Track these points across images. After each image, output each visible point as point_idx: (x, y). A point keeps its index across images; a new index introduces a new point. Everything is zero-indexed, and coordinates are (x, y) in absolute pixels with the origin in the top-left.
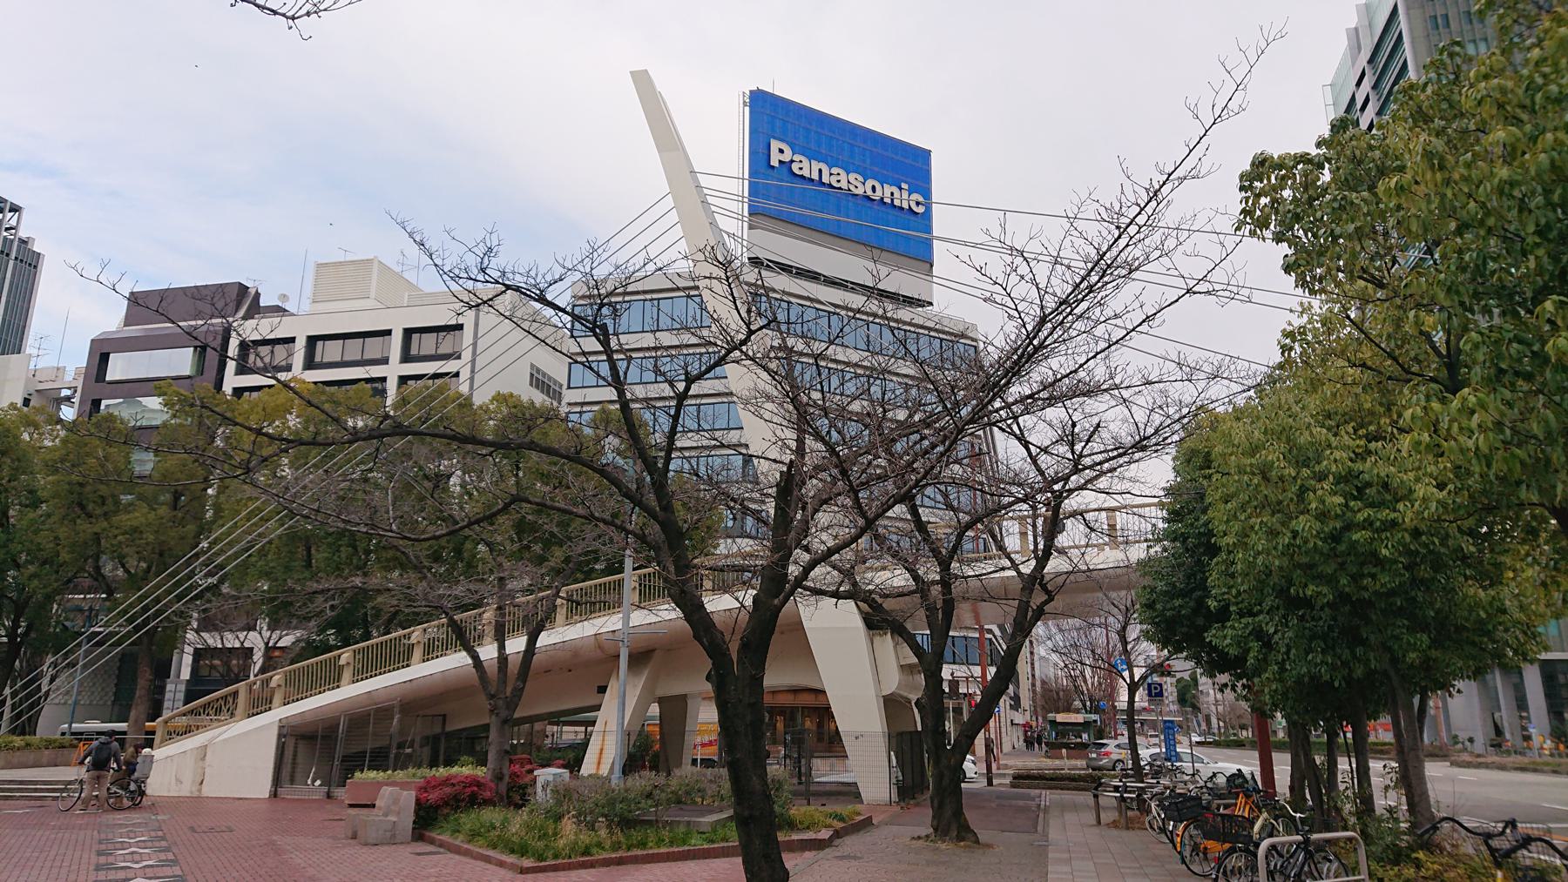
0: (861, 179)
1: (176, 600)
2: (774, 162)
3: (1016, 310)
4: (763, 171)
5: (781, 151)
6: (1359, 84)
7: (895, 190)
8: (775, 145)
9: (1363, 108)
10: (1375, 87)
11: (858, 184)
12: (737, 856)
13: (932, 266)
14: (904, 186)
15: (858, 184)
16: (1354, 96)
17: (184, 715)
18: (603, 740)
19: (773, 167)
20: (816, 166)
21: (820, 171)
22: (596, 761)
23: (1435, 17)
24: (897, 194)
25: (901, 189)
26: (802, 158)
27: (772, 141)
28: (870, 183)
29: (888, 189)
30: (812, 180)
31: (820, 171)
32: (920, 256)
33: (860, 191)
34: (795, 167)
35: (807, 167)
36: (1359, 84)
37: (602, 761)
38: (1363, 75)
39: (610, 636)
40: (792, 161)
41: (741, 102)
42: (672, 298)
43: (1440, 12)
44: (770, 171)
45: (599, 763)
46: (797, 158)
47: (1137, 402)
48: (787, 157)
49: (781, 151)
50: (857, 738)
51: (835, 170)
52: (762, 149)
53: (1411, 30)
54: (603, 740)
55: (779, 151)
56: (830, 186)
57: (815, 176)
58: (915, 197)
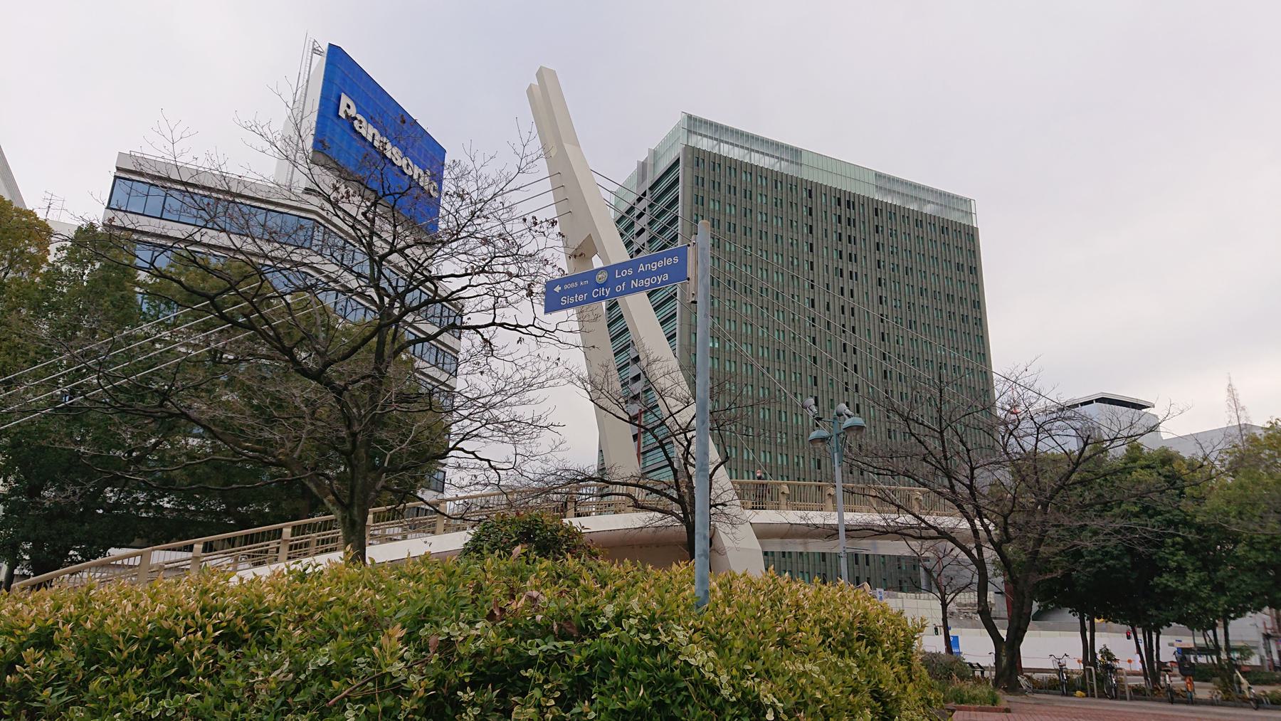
1: (237, 542)
3: (495, 469)
4: (331, 117)
6: (639, 200)
8: (345, 100)
10: (651, 206)
12: (1075, 630)
19: (339, 117)
20: (372, 130)
23: (698, 177)
25: (425, 173)
26: (363, 119)
27: (343, 94)
34: (356, 123)
36: (639, 200)
39: (857, 507)
40: (355, 118)
46: (359, 117)
47: (910, 550)
48: (353, 112)
49: (349, 106)
53: (684, 176)
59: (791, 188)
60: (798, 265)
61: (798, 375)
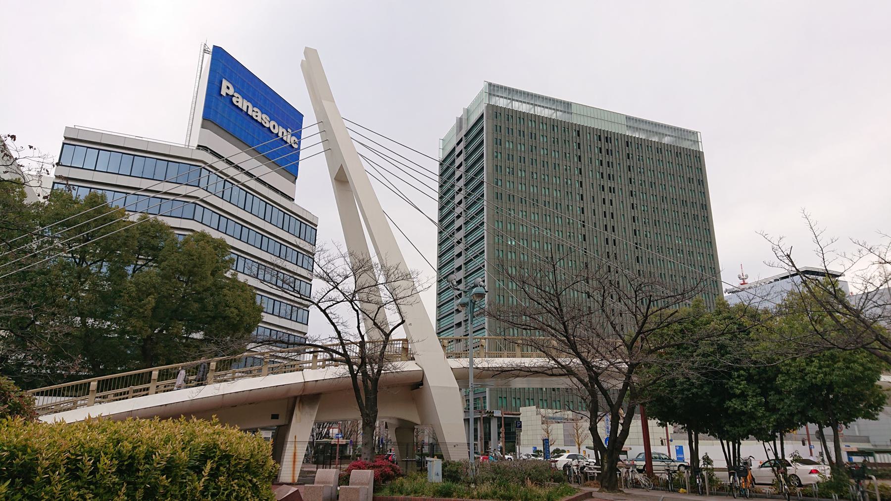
0: (268, 119)
2: (223, 93)
4: (215, 95)
5: (228, 88)
6: (458, 144)
7: (284, 130)
8: (225, 83)
9: (458, 156)
11: (267, 122)
13: (296, 179)
14: (289, 130)
15: (267, 122)
16: (455, 147)
17: (151, 417)
18: (295, 447)
21: (248, 107)
22: (292, 460)
24: (285, 134)
26: (239, 96)
28: (273, 123)
29: (281, 130)
30: (242, 110)
31: (248, 107)
32: (292, 173)
33: (267, 125)
34: (234, 100)
35: (242, 103)
36: (458, 144)
37: (297, 460)
38: (461, 140)
41: (202, 49)
42: (145, 157)
43: (499, 124)
44: (219, 98)
45: (294, 462)
46: (236, 95)
48: (231, 92)
49: (228, 88)
50: (455, 446)
51: (255, 109)
52: (217, 83)
54: (295, 447)
55: (227, 89)
56: (252, 117)
57: (245, 109)
58: (294, 138)
59: (564, 130)
60: (569, 157)
61: (574, 262)
